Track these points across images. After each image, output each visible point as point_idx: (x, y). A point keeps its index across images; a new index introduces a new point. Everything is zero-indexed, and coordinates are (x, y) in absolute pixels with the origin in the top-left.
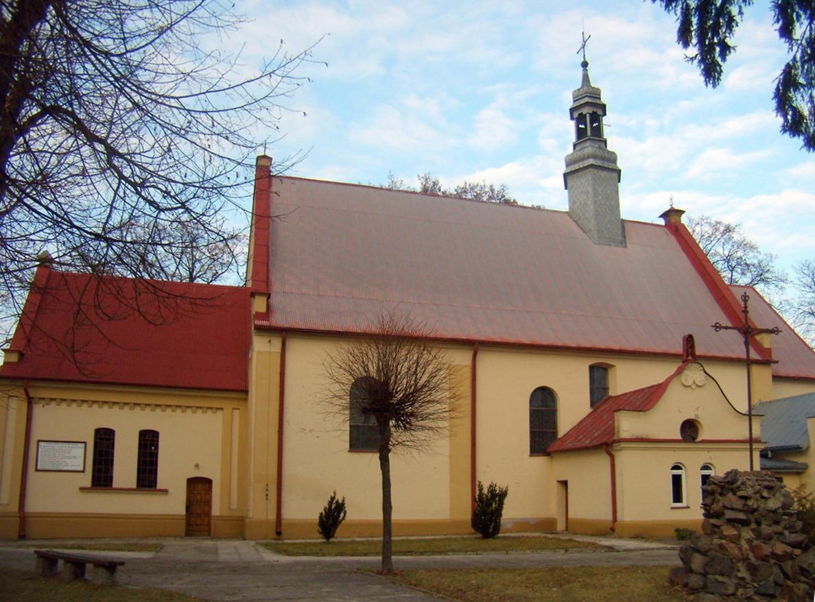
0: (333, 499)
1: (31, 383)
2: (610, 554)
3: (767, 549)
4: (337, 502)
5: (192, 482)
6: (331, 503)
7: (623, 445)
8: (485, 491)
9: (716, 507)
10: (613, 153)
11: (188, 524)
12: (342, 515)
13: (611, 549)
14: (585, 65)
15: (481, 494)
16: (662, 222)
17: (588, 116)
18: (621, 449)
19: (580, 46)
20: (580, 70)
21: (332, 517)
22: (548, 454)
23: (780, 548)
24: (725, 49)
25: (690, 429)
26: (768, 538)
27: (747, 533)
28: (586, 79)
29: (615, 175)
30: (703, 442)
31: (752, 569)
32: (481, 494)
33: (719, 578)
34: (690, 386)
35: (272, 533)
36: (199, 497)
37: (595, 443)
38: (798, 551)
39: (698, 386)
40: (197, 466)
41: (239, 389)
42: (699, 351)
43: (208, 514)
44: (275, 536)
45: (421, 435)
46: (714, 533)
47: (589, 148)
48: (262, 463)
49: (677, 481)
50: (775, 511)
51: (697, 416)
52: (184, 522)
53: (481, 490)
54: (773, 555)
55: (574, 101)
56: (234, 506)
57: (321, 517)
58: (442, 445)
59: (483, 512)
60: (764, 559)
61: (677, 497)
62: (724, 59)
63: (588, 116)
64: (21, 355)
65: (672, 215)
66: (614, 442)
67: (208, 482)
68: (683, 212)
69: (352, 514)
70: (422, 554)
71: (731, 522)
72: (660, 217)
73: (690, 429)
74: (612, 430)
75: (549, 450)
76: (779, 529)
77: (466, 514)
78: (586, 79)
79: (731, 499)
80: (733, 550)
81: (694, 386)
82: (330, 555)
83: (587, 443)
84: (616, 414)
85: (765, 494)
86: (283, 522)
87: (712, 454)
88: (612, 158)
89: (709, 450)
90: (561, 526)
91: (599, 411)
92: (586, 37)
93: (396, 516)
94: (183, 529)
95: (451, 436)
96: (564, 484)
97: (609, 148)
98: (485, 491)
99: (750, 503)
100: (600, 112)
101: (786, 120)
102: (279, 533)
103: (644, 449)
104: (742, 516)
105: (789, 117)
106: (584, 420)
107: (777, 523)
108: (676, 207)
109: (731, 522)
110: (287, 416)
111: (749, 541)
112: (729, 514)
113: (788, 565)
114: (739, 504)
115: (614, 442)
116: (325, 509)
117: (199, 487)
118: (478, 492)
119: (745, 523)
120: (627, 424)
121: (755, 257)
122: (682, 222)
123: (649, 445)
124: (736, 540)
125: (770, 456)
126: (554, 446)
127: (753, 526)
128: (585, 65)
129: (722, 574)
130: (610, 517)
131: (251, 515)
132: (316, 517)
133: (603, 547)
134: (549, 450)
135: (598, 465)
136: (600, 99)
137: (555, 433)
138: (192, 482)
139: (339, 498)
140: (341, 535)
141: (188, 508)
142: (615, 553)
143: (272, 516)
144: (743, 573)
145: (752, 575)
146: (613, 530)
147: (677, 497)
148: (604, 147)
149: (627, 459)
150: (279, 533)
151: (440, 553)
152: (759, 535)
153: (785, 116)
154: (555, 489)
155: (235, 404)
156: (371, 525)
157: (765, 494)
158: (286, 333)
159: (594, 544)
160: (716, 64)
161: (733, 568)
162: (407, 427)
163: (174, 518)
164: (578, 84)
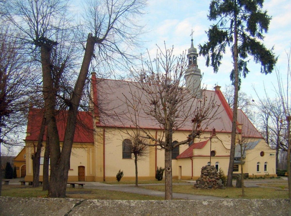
0: (120, 171)
1: (35, 142)
2: (189, 184)
3: (211, 180)
4: (121, 172)
5: (79, 167)
6: (119, 172)
7: (195, 157)
8: (159, 169)
9: (203, 172)
10: (199, 70)
11: (79, 178)
12: (122, 175)
13: (189, 182)
14: (192, 40)
15: (158, 170)
16: (214, 90)
17: (192, 58)
18: (195, 158)
19: (191, 34)
20: (191, 42)
21: (119, 176)
22: (177, 159)
23: (213, 179)
24: (219, 63)
25: (213, 153)
26: (212, 178)
27: (208, 177)
28: (192, 45)
29: (200, 76)
30: (217, 156)
31: (208, 183)
32: (158, 170)
33: (201, 185)
34: (213, 142)
35: (103, 180)
36: (81, 171)
37: (188, 156)
38: (217, 180)
39: (216, 142)
40: (81, 163)
41: (92, 142)
42: (216, 130)
43: (84, 175)
44: (103, 181)
45: (144, 157)
46: (202, 177)
47: (193, 68)
48: (99, 162)
49: (258, 166)
50: (213, 173)
51: (215, 150)
52: (78, 178)
53: (158, 169)
54: (212, 181)
55: (189, 52)
56: (91, 173)
57: (117, 176)
58: (148, 159)
59: (159, 174)
60: (210, 181)
61: (258, 170)
62: (219, 66)
63: (192, 58)
64: (31, 134)
65: (217, 88)
66: (193, 156)
67: (84, 167)
68: (220, 87)
69: (125, 175)
70: (143, 184)
71: (205, 175)
72: (214, 88)
73: (213, 153)
74: (192, 153)
75: (177, 158)
76: (214, 176)
77: (154, 174)
78: (192, 45)
79: (205, 171)
80: (205, 180)
81: (215, 142)
82: (121, 184)
83: (186, 156)
84: (194, 149)
85: (212, 170)
86: (105, 177)
87: (219, 159)
88: (199, 71)
89: (218, 158)
90: (179, 178)
91: (191, 147)
92: (193, 31)
93: (138, 175)
94: (78, 180)
95: (150, 158)
96: (181, 167)
97: (199, 68)
98: (159, 169)
99: (209, 171)
100: (196, 56)
101: (233, 82)
102: (104, 180)
103: (201, 158)
104: (207, 174)
105: (234, 81)
106: (187, 150)
107: (214, 175)
108: (219, 85)
109: (205, 175)
110: (105, 150)
111: (208, 178)
112: (204, 174)
113: (214, 183)
114: (207, 172)
115: (193, 156)
116: (118, 174)
117: (81, 168)
118: (157, 169)
119: (208, 175)
120: (196, 152)
121: (246, 97)
122: (220, 90)
123: (222, 157)
124: (205, 178)
125: (236, 159)
126: (178, 157)
127: (209, 176)
128: (192, 40)
129: (202, 184)
130: (191, 175)
131: (97, 175)
132: (116, 176)
133: (187, 182)
134: (177, 158)
135: (189, 162)
136: (196, 52)
137: (178, 153)
138: (79, 167)
139: (121, 171)
140: (122, 180)
141: (79, 174)
142: (190, 184)
143: (103, 176)
144: (206, 184)
145: (208, 184)
146: (192, 178)
147: (258, 170)
148: (197, 67)
149: (195, 160)
150: (104, 180)
151: (148, 184)
152: (210, 177)
153: (233, 81)
154: (178, 168)
155: (91, 146)
156: (131, 178)
157: (212, 170)
158: (105, 128)
159: (185, 181)
160: (217, 67)
161: (204, 183)
162: (141, 155)
163: (75, 177)
164: (190, 47)
